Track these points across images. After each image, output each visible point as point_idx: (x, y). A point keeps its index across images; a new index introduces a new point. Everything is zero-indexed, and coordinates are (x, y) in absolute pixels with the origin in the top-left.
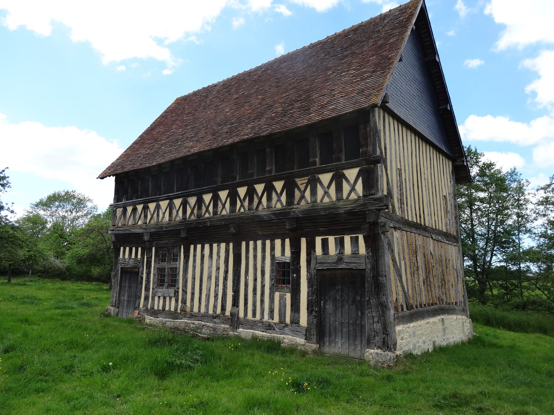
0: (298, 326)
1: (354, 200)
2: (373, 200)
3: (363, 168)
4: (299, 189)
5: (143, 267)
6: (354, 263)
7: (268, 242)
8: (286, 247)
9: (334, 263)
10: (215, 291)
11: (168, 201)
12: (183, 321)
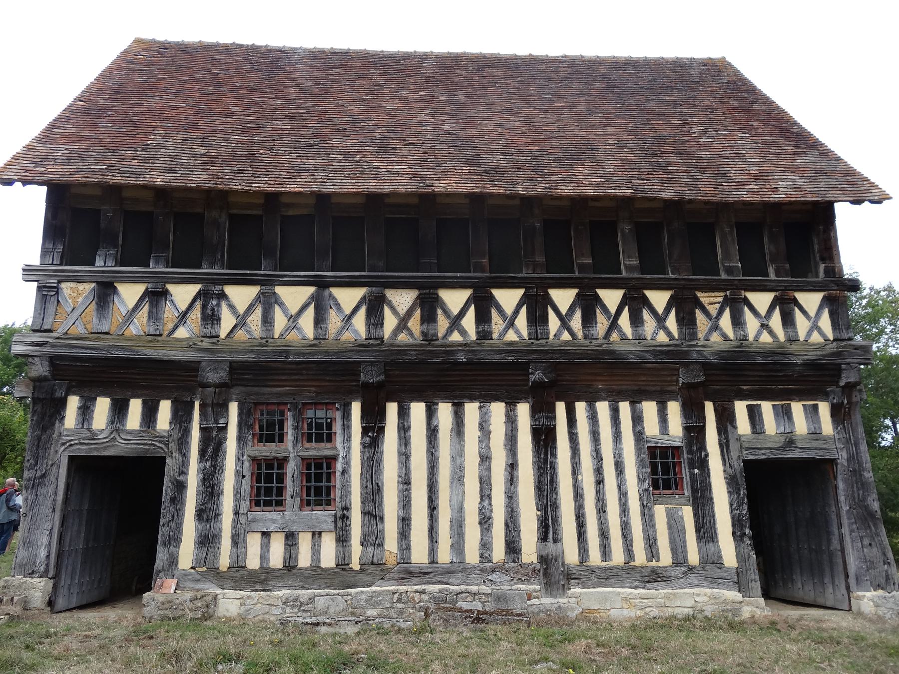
0: (720, 568)
1: (818, 344)
2: (852, 348)
3: (830, 294)
4: (285, 310)
5: (185, 455)
6: (816, 449)
7: (625, 408)
8: (669, 417)
9: (778, 449)
10: (480, 510)
11: (311, 290)
12: (379, 589)
